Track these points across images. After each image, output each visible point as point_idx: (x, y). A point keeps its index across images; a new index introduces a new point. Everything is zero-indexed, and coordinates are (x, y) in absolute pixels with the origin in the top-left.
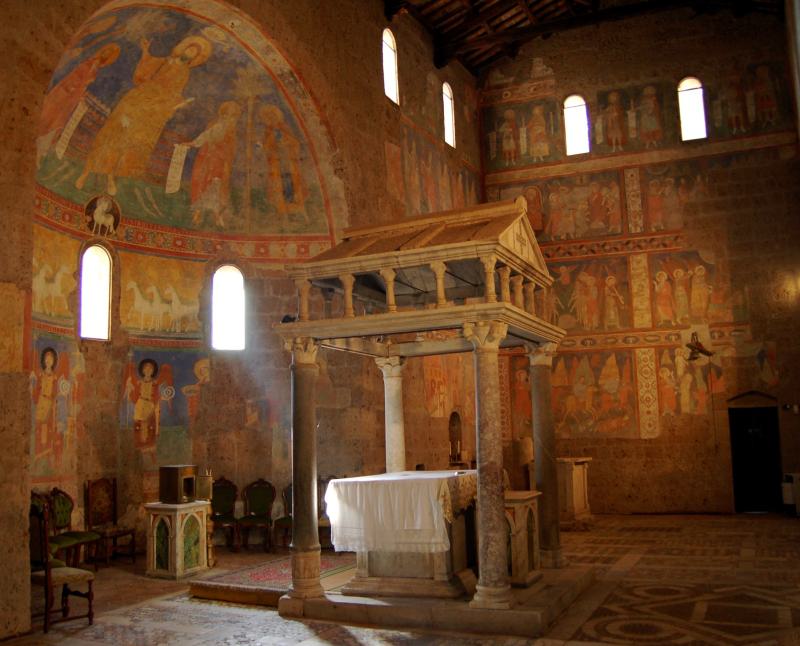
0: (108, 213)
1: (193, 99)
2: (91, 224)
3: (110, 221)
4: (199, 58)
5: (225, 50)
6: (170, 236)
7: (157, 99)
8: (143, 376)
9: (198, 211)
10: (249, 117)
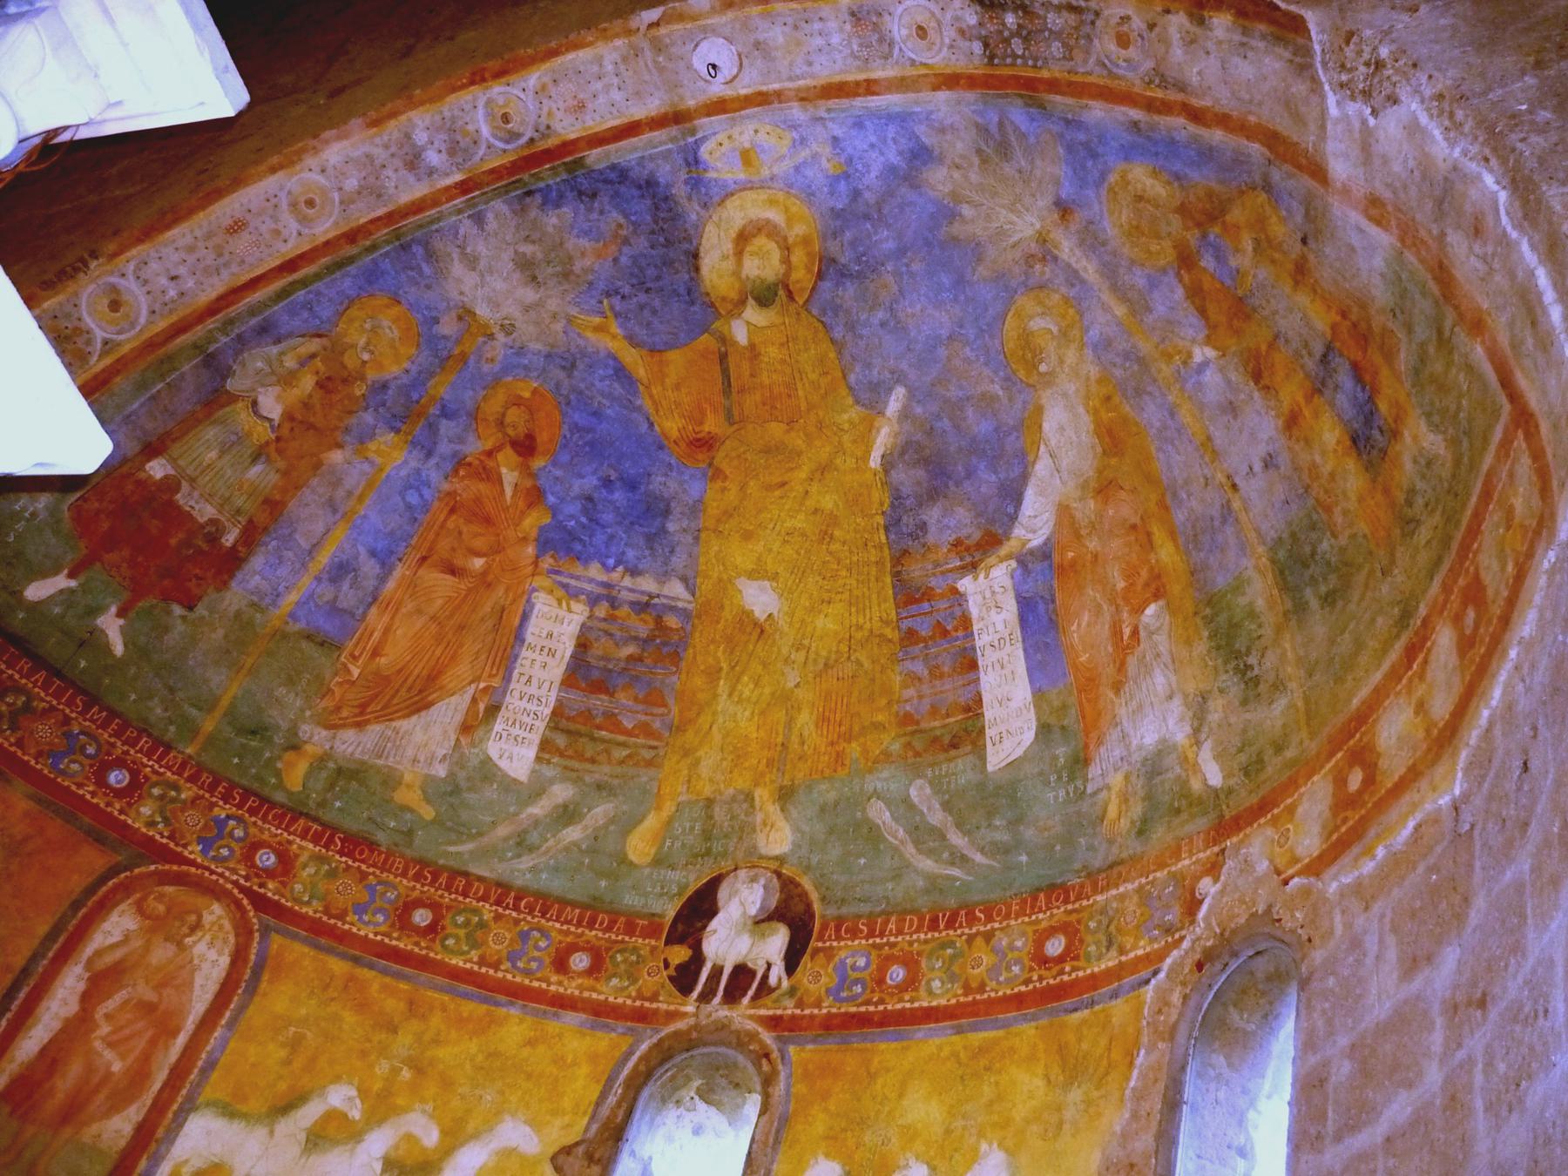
1: (899, 393)
4: (798, 257)
5: (829, 165)
7: (803, 474)
9: (1117, 780)
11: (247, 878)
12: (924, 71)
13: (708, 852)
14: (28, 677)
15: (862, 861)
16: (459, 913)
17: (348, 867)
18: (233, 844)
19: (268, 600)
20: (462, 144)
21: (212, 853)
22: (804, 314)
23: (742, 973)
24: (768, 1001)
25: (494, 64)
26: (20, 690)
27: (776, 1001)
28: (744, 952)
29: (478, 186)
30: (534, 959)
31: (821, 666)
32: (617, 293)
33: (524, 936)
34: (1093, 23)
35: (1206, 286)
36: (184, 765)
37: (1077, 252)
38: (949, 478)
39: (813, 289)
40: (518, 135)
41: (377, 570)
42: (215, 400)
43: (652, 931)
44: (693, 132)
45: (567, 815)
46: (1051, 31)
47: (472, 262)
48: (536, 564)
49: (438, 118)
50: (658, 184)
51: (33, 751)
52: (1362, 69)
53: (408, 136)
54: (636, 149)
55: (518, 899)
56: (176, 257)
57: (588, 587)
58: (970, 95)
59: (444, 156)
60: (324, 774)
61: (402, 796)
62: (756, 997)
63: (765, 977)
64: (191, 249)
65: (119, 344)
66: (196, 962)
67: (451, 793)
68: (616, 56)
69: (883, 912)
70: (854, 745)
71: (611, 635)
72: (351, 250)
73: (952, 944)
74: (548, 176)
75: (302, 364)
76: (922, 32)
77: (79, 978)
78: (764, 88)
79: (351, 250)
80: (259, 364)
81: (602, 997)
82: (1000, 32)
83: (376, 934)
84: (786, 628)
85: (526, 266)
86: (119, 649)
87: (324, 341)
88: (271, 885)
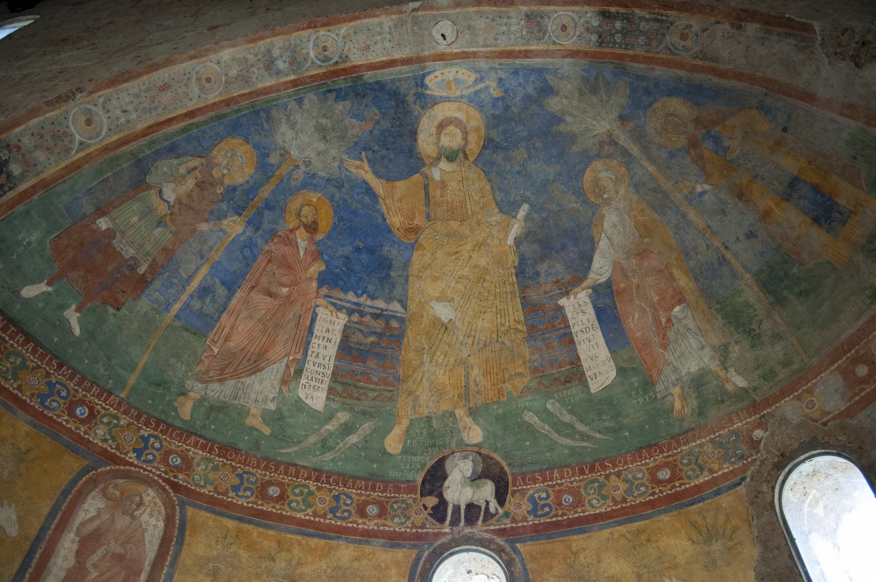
0: (476, 479)
1: (526, 207)
2: (439, 512)
3: (487, 491)
4: (472, 137)
5: (496, 93)
6: (638, 471)
7: (468, 247)
9: (677, 391)
10: (646, 163)
11: (166, 473)
12: (559, 47)
13: (434, 445)
14: (23, 345)
15: (528, 443)
16: (296, 487)
17: (225, 464)
18: (155, 452)
19: (163, 307)
20: (298, 60)
21: (143, 458)
22: (473, 166)
23: (471, 507)
24: (493, 521)
25: (323, 19)
26: (17, 354)
27: (498, 521)
28: (470, 496)
29: (303, 83)
30: (346, 511)
31: (481, 345)
32: (370, 149)
33: (337, 498)
34: (668, 28)
35: (706, 156)
36: (120, 404)
37: (629, 141)
38: (552, 249)
39: (479, 153)
40: (331, 59)
41: (226, 292)
43: (411, 490)
44: (423, 68)
45: (347, 429)
46: (641, 31)
47: (292, 125)
48: (318, 292)
49: (287, 43)
50: (399, 94)
51: (28, 393)
52: (854, 45)
53: (269, 51)
54: (392, 74)
55: (328, 477)
56: (128, 99)
57: (347, 305)
58: (583, 62)
59: (287, 65)
60: (203, 410)
61: (250, 421)
62: (484, 520)
63: (487, 508)
64: (137, 96)
65: (89, 146)
66: (144, 526)
67: (279, 419)
68: (391, 23)
69: (548, 469)
70: (507, 384)
71: (361, 331)
72: (226, 110)
73: (597, 480)
74: (342, 83)
75: (189, 172)
76: (564, 28)
77: (73, 541)
78: (467, 50)
79: (226, 110)
80: (165, 169)
81: (392, 529)
82: (611, 30)
83: (248, 503)
84: (460, 326)
85: (322, 132)
86: (77, 331)
87: (203, 160)
88: (180, 476)
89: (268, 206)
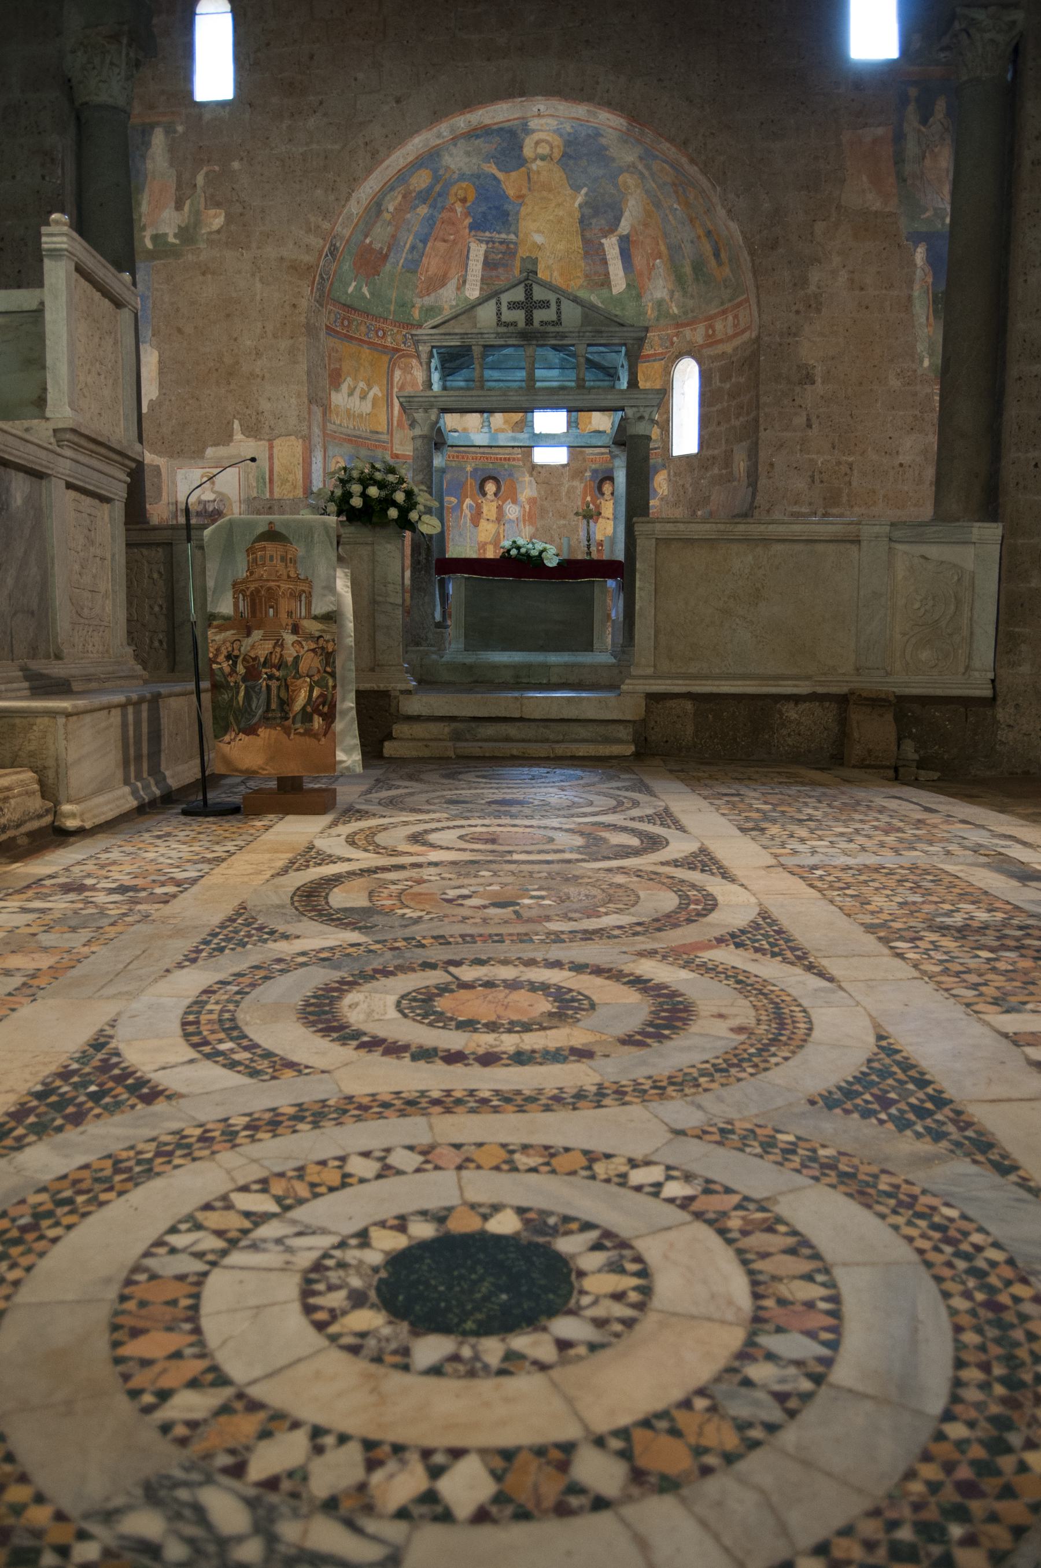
4: (556, 150)
8: (603, 494)
9: (650, 304)
42: (379, 212)
47: (451, 155)
85: (468, 154)
89: (439, 195)
